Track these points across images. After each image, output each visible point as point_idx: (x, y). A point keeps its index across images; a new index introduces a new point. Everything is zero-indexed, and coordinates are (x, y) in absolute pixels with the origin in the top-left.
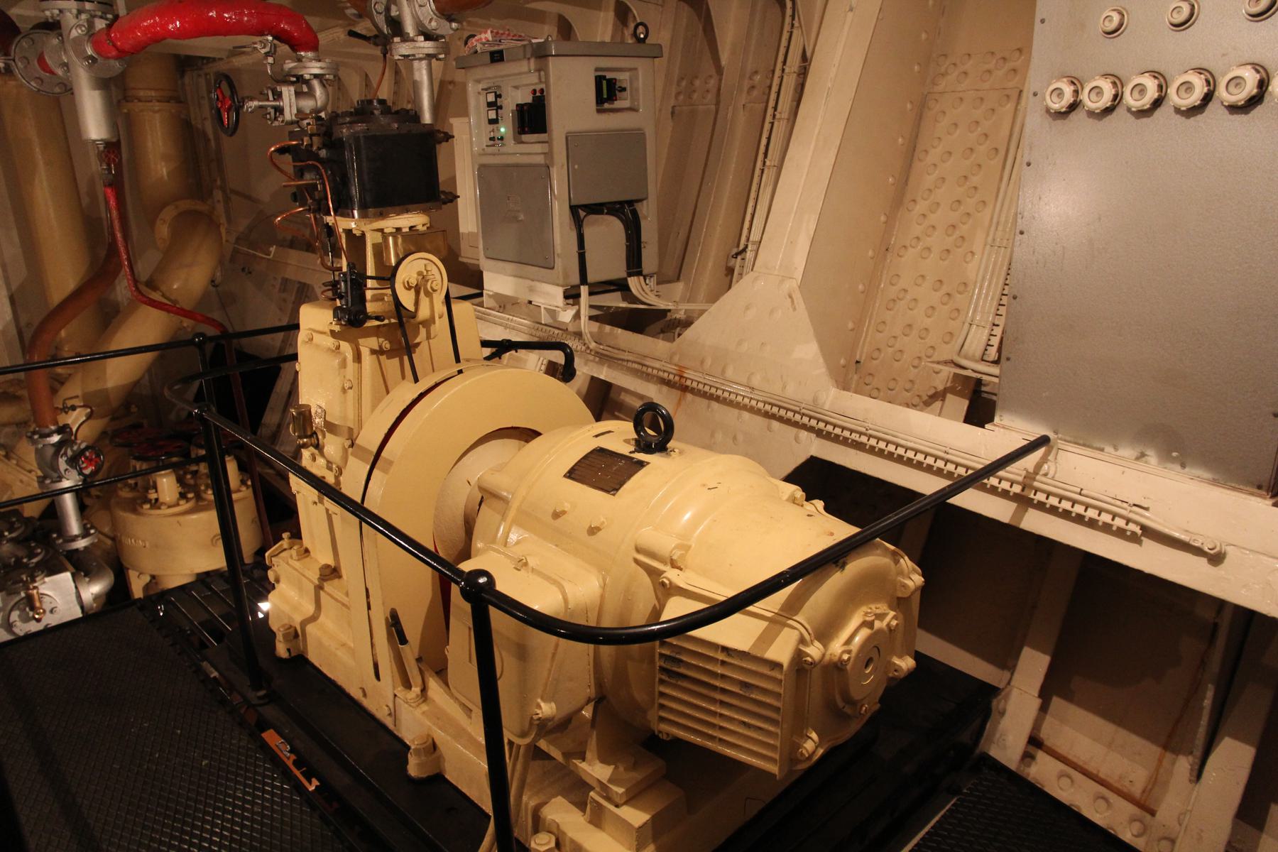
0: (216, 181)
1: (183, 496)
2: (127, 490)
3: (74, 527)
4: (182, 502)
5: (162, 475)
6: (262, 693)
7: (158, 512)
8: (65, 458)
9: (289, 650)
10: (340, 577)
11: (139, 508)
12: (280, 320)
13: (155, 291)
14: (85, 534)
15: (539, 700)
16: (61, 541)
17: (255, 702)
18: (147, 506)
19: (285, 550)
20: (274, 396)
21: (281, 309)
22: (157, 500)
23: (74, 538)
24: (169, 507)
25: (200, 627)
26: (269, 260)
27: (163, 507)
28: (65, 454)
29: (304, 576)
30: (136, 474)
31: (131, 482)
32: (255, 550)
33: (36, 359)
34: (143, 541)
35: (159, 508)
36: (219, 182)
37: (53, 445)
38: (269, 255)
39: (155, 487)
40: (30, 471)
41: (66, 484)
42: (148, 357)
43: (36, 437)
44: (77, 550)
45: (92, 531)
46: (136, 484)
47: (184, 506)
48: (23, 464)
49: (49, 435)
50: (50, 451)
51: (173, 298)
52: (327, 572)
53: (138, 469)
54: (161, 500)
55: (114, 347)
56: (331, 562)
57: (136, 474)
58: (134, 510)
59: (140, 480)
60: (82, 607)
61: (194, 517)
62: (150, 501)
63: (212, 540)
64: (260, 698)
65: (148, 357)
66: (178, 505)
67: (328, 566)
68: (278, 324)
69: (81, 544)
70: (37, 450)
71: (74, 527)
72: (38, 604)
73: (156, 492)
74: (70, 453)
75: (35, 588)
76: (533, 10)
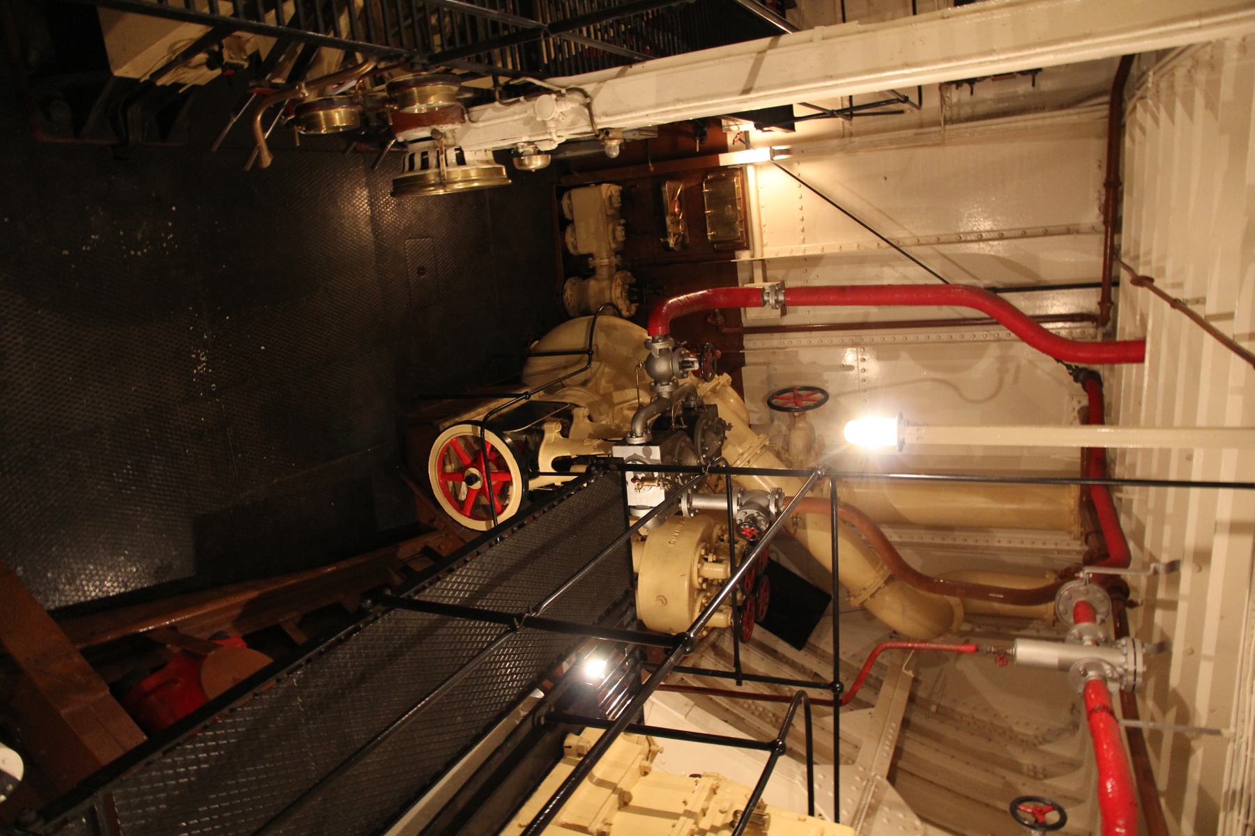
0: (979, 627)
1: (705, 580)
2: (720, 534)
3: (698, 503)
4: (700, 580)
5: (727, 569)
6: (543, 721)
7: (697, 561)
8: (756, 515)
9: (570, 747)
10: (619, 809)
11: (703, 544)
12: (844, 653)
13: (885, 582)
14: (690, 510)
15: (303, 85)
16: (690, 491)
17: (537, 715)
18: (703, 552)
19: (650, 745)
20: (774, 637)
21: (854, 655)
22: (706, 560)
23: (689, 502)
24: (698, 570)
25: (533, 40)
26: (902, 666)
27: (700, 565)
28: (760, 515)
29: (627, 772)
30: (732, 542)
31: (726, 537)
32: (645, 621)
33: (840, 510)
34: (675, 543)
35: (699, 562)
36: (978, 630)
37: (768, 506)
38: (906, 668)
39: (717, 561)
40: (749, 462)
41: (735, 508)
42: (828, 564)
43: (777, 497)
44: (680, 502)
45: (692, 515)
46: (723, 540)
47: (697, 581)
48: (756, 457)
49: (776, 505)
50: (763, 502)
51: (876, 595)
52: (626, 800)
53: (736, 546)
54: (706, 564)
55: (842, 541)
56: (632, 803)
57: (732, 542)
58: (702, 540)
59: (725, 545)
60: (634, 507)
61: (686, 584)
62: (707, 554)
63: (663, 597)
64: (539, 719)
65: (828, 564)
66: (699, 576)
67: (630, 800)
68: (841, 651)
69: (684, 506)
70: (766, 493)
71: (698, 503)
72: (645, 483)
73: (714, 561)
74: (759, 518)
75: (659, 485)
76: (1192, 96)
